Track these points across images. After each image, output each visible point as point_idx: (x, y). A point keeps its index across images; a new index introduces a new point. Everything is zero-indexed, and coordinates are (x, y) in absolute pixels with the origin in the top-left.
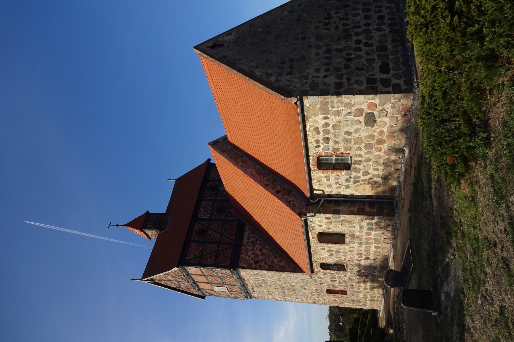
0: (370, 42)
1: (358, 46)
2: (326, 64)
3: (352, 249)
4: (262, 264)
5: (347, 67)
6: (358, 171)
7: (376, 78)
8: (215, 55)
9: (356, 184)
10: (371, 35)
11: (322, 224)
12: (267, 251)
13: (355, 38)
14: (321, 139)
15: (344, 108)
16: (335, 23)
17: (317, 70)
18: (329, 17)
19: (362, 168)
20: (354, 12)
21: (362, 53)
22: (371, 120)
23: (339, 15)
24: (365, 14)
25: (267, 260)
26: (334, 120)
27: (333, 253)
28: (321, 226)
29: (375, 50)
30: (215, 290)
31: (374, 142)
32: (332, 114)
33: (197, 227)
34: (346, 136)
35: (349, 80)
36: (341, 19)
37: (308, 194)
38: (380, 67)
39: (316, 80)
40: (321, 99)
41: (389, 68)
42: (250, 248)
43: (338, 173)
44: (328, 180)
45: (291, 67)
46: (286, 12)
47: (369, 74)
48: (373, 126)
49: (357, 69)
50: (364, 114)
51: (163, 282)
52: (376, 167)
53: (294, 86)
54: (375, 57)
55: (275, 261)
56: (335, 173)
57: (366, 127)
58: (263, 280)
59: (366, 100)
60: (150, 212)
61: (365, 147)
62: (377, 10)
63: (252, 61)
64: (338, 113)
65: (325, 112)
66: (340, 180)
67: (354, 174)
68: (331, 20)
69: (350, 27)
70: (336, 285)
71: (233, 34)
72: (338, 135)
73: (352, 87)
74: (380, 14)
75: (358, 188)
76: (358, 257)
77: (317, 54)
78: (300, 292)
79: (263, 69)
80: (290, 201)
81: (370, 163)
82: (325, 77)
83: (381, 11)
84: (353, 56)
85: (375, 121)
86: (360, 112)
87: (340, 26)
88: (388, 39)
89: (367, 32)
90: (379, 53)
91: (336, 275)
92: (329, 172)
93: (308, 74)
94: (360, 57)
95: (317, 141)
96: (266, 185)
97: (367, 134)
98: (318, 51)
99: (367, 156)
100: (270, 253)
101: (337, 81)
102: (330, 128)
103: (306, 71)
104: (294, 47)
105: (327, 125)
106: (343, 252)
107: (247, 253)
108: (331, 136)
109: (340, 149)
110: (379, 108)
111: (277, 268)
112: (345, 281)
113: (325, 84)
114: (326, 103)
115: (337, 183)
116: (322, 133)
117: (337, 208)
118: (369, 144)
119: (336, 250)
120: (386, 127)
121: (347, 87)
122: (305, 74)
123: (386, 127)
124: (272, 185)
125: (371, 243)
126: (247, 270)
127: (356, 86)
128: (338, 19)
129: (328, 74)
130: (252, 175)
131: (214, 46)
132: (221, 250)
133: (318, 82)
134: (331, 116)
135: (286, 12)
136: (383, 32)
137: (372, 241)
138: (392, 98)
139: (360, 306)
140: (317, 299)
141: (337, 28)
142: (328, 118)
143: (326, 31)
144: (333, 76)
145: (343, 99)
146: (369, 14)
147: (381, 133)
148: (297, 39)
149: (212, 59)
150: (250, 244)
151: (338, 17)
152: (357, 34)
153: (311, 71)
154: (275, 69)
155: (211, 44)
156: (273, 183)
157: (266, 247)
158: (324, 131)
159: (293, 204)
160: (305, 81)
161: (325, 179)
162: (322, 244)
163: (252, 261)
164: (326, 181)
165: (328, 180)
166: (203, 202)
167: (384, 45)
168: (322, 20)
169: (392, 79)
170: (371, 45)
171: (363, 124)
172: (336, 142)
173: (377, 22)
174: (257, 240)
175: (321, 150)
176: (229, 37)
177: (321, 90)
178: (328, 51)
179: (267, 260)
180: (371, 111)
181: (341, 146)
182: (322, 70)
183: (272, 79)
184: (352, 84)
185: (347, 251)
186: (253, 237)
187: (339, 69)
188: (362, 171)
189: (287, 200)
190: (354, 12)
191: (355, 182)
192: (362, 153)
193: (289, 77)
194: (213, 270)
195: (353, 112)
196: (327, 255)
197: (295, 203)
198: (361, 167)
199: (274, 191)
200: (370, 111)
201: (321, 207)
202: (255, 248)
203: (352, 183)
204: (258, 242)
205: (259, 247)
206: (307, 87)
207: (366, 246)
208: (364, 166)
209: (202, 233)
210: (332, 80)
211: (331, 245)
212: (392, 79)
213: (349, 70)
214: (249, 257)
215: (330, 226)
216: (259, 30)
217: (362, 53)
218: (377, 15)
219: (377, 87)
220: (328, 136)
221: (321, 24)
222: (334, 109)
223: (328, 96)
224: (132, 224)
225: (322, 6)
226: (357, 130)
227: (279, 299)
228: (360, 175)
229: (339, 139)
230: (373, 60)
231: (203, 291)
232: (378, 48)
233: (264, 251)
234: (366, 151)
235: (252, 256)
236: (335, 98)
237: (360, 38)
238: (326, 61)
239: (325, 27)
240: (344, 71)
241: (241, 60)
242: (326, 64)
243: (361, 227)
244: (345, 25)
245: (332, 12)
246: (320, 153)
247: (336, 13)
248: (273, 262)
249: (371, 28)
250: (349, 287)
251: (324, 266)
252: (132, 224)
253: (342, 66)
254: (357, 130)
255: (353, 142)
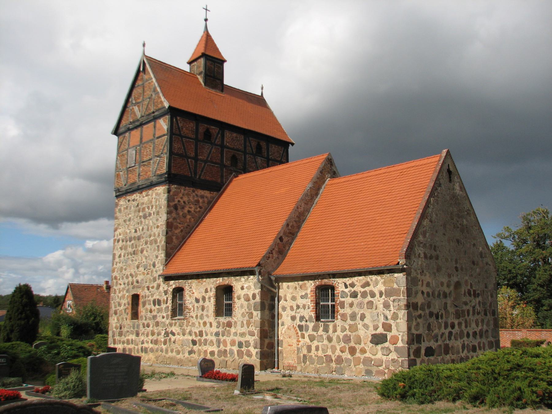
0: (453, 338)
1: (449, 326)
2: (433, 293)
3: (208, 325)
4: (174, 215)
5: (431, 314)
6: (315, 329)
7: (421, 344)
8: (441, 174)
9: (297, 328)
10: (459, 339)
11: (245, 290)
12: (188, 221)
13: (456, 322)
14: (355, 289)
15: (392, 312)
16: (470, 301)
17: (428, 284)
18: (476, 295)
19: (319, 334)
20: (480, 321)
21: (443, 330)
22: (378, 339)
23: (478, 305)
24: (478, 333)
25: (178, 221)
26: (379, 303)
27: (201, 302)
28: (242, 288)
29: (445, 343)
30: (129, 150)
31: (352, 344)
32: (385, 301)
33: (214, 130)
34: (359, 315)
35: (420, 316)
36: (474, 307)
37: (281, 271)
38: (431, 347)
39: (420, 283)
40: (403, 288)
41: (430, 356)
42: (191, 199)
43: (311, 308)
44: (302, 297)
45: (431, 258)
46: (481, 249)
47: (425, 337)
48: (371, 342)
49: (429, 324)
50: (386, 332)
51: (139, 83)
52: (320, 349)
53: (414, 261)
54: (439, 343)
55: (177, 231)
56: (312, 305)
57: (370, 335)
58: (150, 215)
59: (401, 334)
60: (225, 65)
61: (346, 336)
62: (482, 345)
63: (437, 215)
64: (386, 306)
65: (389, 293)
66: (302, 310)
67: (311, 325)
68: (473, 297)
69: (466, 317)
70: (148, 307)
71: (461, 192)
72: (361, 307)
73: (414, 319)
74: (478, 348)
75: (293, 330)
76: (195, 333)
77: (442, 284)
78: (132, 261)
79: (430, 228)
80: (272, 253)
81: (326, 342)
82: (423, 293)
83: (480, 349)
84: (440, 321)
85: (377, 344)
86: (387, 327)
87: (468, 307)
88: (455, 355)
89: (461, 335)
90: (443, 347)
91: (164, 306)
92: (313, 298)
93: (426, 275)
94: (440, 328)
95: (353, 285)
96: (288, 225)
97: (362, 337)
98: (445, 285)
99: (334, 339)
100: (186, 224)
101: (419, 304)
102: (369, 298)
103: (427, 273)
104: (449, 260)
105: (373, 295)
106: (202, 315)
107: (187, 195)
108: (360, 300)
109: (343, 310)
110: (392, 347)
111: (170, 233)
112: (155, 317)
113: (416, 293)
114: (398, 294)
115: (298, 307)
116: (362, 290)
117: (267, 307)
118: (350, 339)
119: (206, 306)
120: (371, 356)
121: (413, 315)
122: (425, 271)
123: (371, 356)
124: (288, 231)
125: (219, 346)
126: (166, 195)
127: (414, 323)
128: (473, 304)
129: (425, 295)
130: (298, 208)
131: (449, 172)
132: (188, 161)
133: (417, 285)
134: (384, 299)
135: (481, 249)
136: (461, 350)
137: (222, 347)
138: (403, 359)
139: (113, 336)
140: (121, 281)
141: (466, 304)
142: (381, 296)
143: (463, 293)
144: (423, 301)
145: (403, 311)
146: (478, 337)
147: (363, 351)
148: (456, 262)
149: (438, 171)
150: (196, 199)
151: (475, 305)
152: (460, 324)
153: (427, 278)
154: (429, 240)
155: (451, 169)
156: (290, 233)
157: (193, 220)
158: (365, 292)
159: (269, 257)
160: (419, 272)
161: (303, 294)
162: (214, 290)
163: (176, 202)
164: (300, 294)
165: (302, 297)
166: (243, 137)
167: (450, 352)
168: (474, 288)
169: (420, 359)
170: (450, 339)
171: (374, 332)
172: (351, 305)
173: (471, 345)
174: (201, 207)
175: (342, 289)
176: (458, 188)
177: (412, 289)
178: (445, 295)
179: (178, 221)
180: (388, 340)
181: (348, 311)
182: (429, 290)
183: (421, 238)
184: (416, 319)
185: (205, 319)
186: (204, 202)
187: (429, 307)
188: (315, 333)
189: (273, 249)
190: (480, 321)
191: (301, 327)
192: (339, 332)
193: (422, 255)
194: (165, 151)
195: (388, 322)
196: (197, 295)
197: (270, 259)
198: (321, 332)
199: (282, 235)
200: (388, 338)
201: (268, 289)
202: (192, 206)
203: (299, 323)
204: (199, 209)
205: (192, 210)
206: (414, 274)
207: (215, 341)
208: (321, 336)
209: (208, 136)
210: (420, 300)
211: (213, 300)
212: (420, 359)
213: (428, 317)
214: (182, 198)
215: (242, 299)
216: (464, 220)
217: (443, 330)
218: (477, 345)
219: (414, 344)
220: (359, 296)
221: (469, 287)
222: (391, 303)
223: (406, 295)
224: (208, 39)
225: (486, 287)
226: (366, 326)
227: (117, 233)
228: (310, 332)
229: (355, 309)
230: (437, 341)
231: (127, 134)
232: (447, 346)
233: (189, 217)
234: (341, 337)
235: (182, 201)
236: (403, 303)
237: (456, 327)
238: (436, 293)
239: (467, 291)
240: (427, 311)
241: (438, 204)
242: (433, 293)
243: (243, 335)
244: (468, 311)
245: (480, 298)
246: (338, 288)
247: (479, 302)
248: (176, 228)
249: (465, 338)
250: (146, 322)
251: (179, 292)
252: (208, 39)
253: (432, 309)
254: (366, 326)
255: (352, 323)
